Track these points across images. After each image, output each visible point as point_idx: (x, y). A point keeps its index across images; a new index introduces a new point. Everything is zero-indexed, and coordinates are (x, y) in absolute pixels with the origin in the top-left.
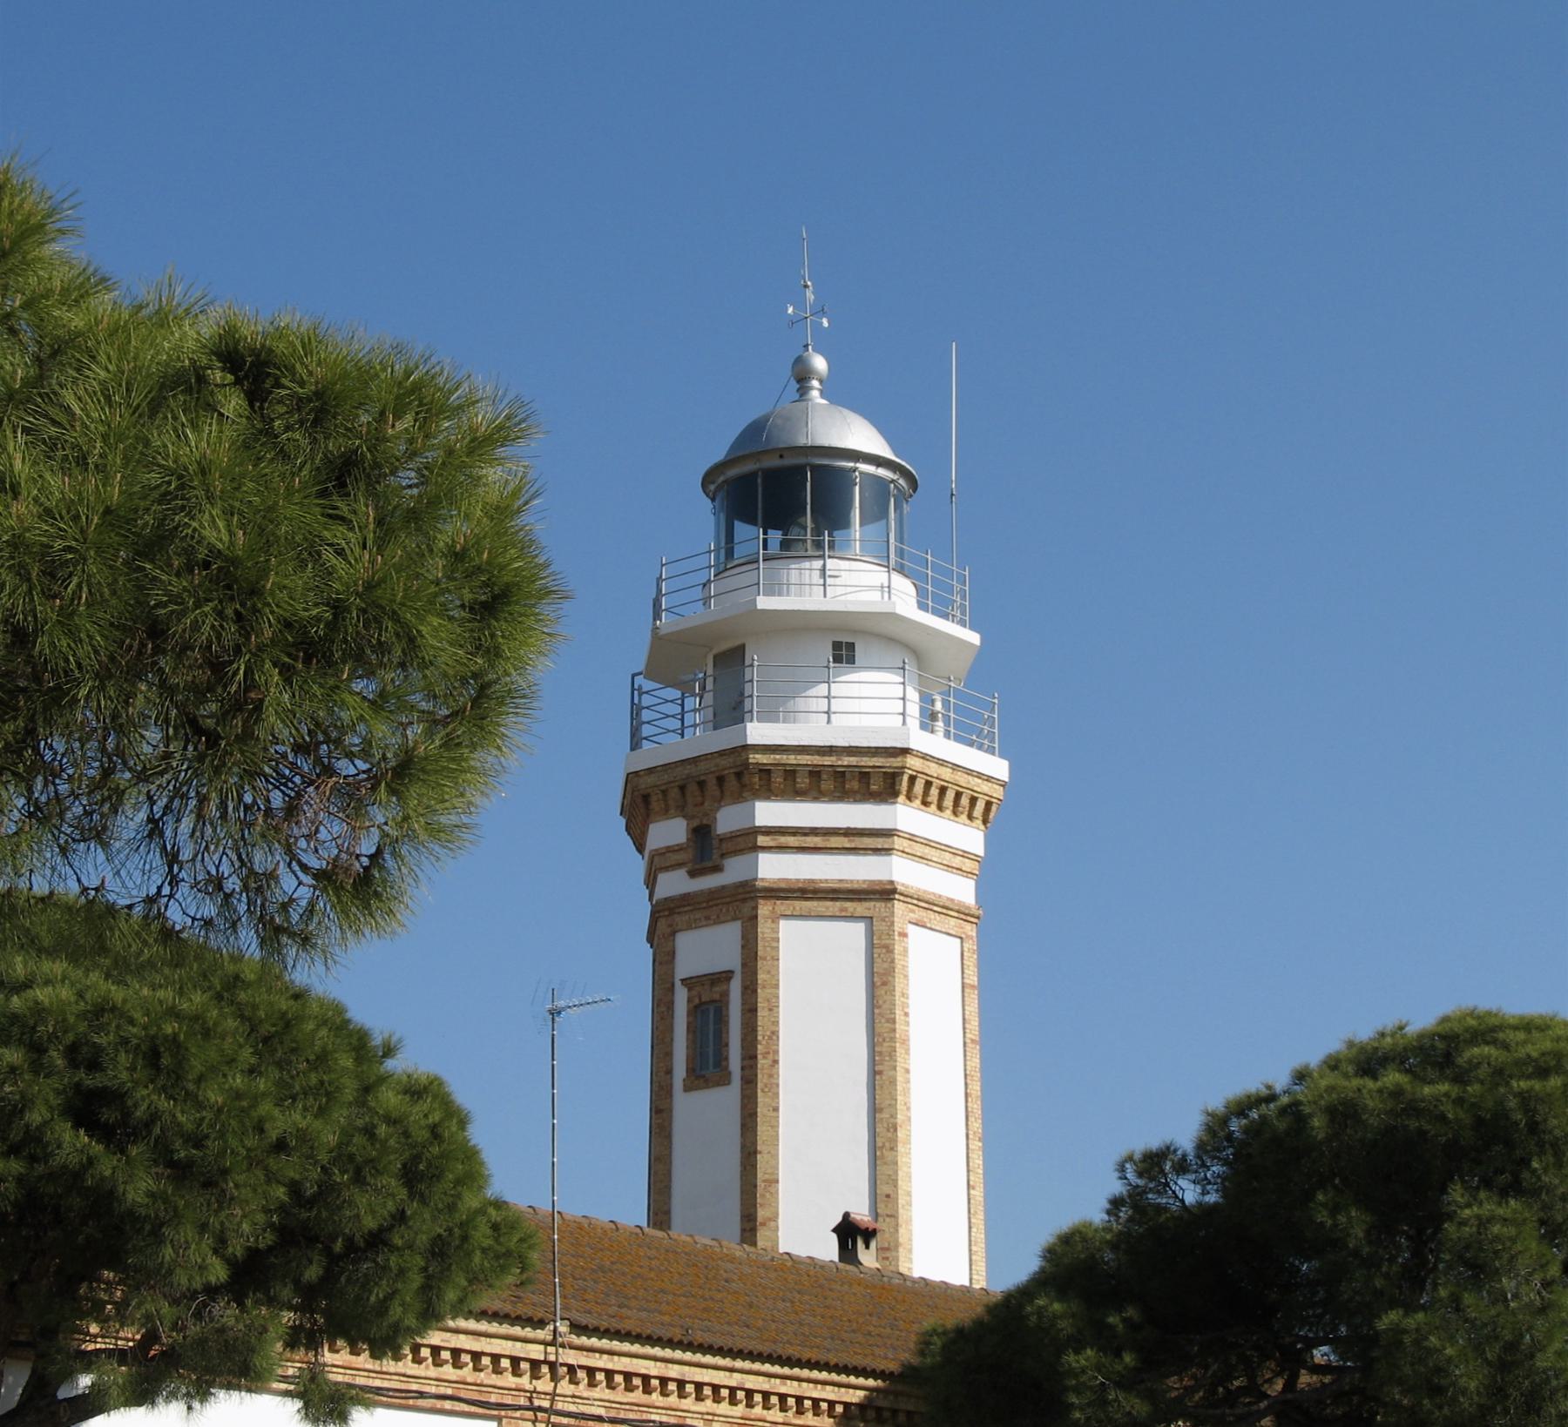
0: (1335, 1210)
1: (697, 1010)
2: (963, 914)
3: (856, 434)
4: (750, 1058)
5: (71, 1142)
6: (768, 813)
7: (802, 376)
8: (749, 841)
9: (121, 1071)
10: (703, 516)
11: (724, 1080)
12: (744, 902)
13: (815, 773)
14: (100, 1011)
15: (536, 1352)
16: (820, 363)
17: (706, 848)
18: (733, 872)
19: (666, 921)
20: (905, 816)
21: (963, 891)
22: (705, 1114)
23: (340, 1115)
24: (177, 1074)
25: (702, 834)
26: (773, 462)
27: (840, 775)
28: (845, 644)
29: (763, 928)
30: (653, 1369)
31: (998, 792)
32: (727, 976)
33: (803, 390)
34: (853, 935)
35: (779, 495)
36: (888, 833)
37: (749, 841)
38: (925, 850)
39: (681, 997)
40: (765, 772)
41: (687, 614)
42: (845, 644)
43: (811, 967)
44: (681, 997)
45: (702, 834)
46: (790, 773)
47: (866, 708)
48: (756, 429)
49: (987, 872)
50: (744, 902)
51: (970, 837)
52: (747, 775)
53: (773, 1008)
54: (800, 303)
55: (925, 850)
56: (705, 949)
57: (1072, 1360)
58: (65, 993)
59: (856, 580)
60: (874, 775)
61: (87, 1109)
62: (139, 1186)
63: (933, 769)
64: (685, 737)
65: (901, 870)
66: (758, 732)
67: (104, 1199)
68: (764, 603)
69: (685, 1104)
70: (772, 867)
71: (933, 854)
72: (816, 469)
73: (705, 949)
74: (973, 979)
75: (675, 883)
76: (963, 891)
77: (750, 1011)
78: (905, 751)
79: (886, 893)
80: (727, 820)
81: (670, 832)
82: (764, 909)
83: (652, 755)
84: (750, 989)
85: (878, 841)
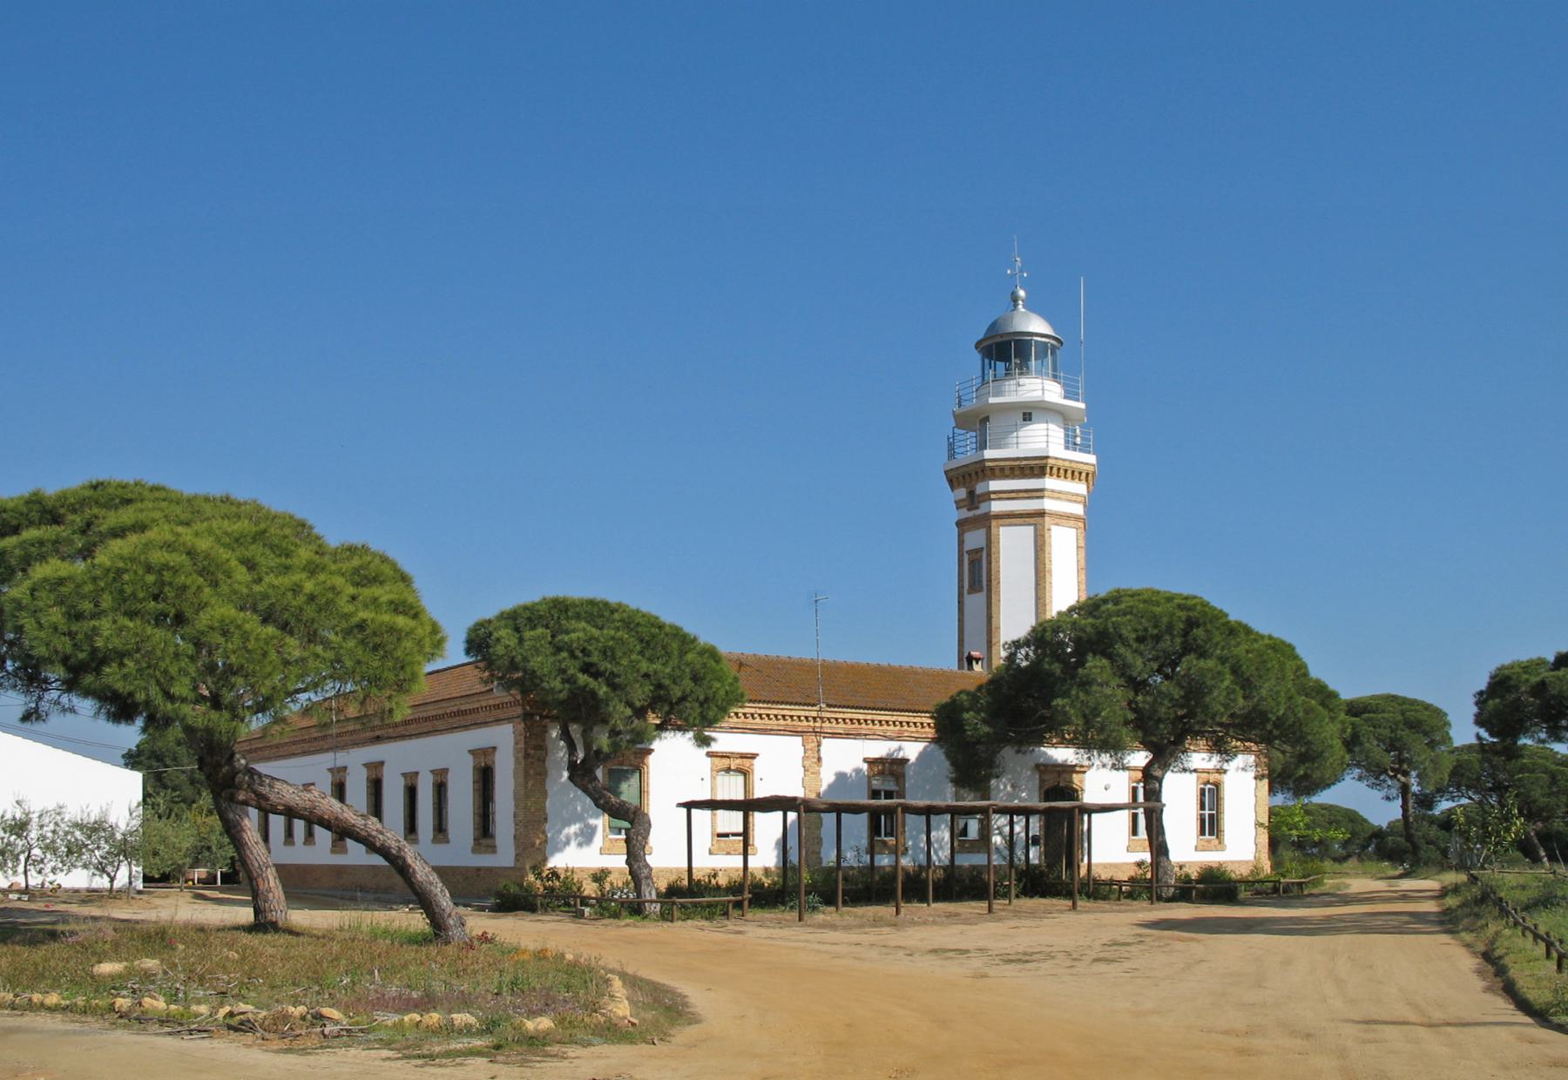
0: (1050, 664)
1: (972, 563)
2: (1077, 518)
3: (1036, 325)
4: (989, 581)
5: (583, 679)
6: (994, 485)
7: (1015, 299)
8: (988, 496)
9: (595, 658)
10: (976, 357)
11: (981, 590)
12: (986, 521)
13: (1012, 468)
14: (591, 639)
15: (814, 714)
16: (1022, 293)
17: (973, 500)
18: (982, 510)
19: (962, 525)
20: (1050, 483)
21: (1078, 510)
22: (975, 601)
23: (675, 661)
24: (614, 658)
25: (971, 493)
26: (999, 340)
27: (1022, 468)
28: (1028, 413)
29: (993, 531)
30: (861, 717)
31: (1091, 469)
32: (980, 550)
33: (1016, 305)
34: (1028, 532)
35: (1006, 351)
36: (1042, 490)
37: (988, 496)
38: (1058, 495)
39: (966, 557)
40: (992, 469)
41: (971, 404)
42: (1028, 413)
43: (1012, 544)
44: (966, 557)
45: (971, 493)
46: (1002, 469)
47: (1044, 439)
48: (994, 325)
49: (1090, 503)
50: (986, 521)
51: (1080, 488)
52: (984, 471)
53: (998, 562)
54: (1013, 269)
55: (1058, 495)
56: (975, 539)
57: (966, 716)
58: (581, 634)
59: (1038, 387)
60: (1037, 467)
61: (587, 668)
62: (603, 690)
63: (1060, 463)
64: (967, 455)
65: (1048, 504)
66: (989, 454)
67: (593, 694)
68: (992, 400)
69: (968, 598)
70: (997, 507)
71: (1064, 497)
72: (1016, 342)
73: (975, 539)
74: (1082, 544)
75: (965, 513)
76: (1078, 510)
77: (989, 563)
78: (1047, 457)
79: (1041, 514)
80: (980, 489)
81: (962, 493)
82: (994, 523)
83: (954, 464)
84: (989, 555)
85: (1039, 493)
